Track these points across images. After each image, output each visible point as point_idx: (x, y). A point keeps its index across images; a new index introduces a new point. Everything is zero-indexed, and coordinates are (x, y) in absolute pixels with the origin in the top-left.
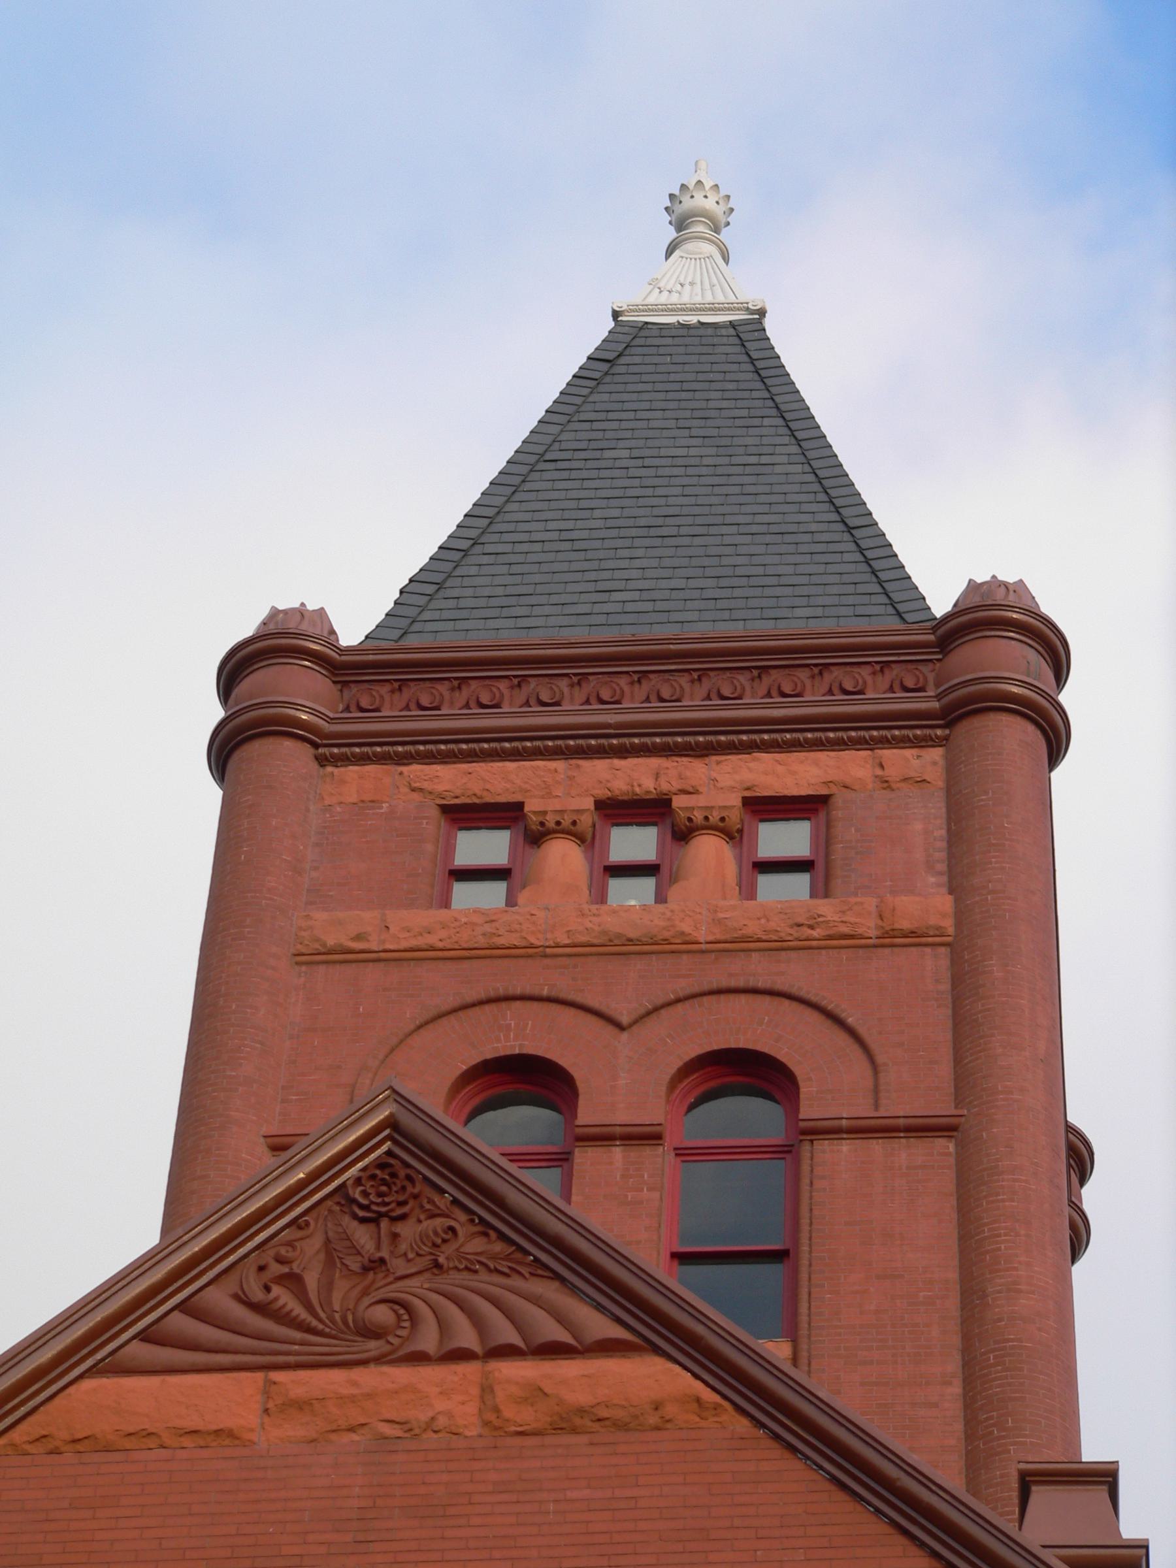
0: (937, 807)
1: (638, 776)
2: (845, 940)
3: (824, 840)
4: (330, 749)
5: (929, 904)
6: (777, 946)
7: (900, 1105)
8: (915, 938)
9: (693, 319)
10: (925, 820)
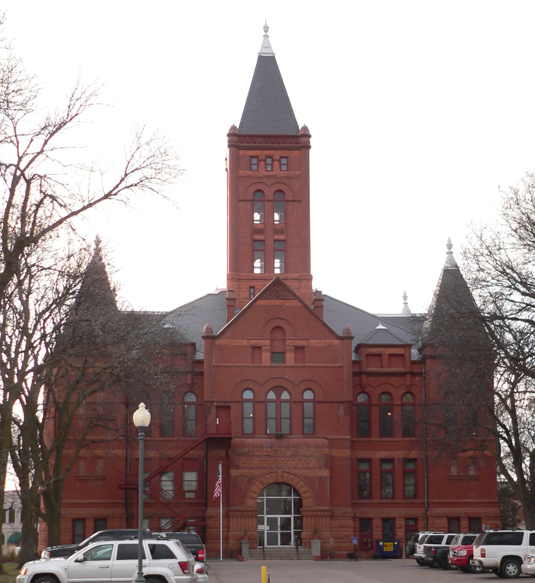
1: (267, 152)
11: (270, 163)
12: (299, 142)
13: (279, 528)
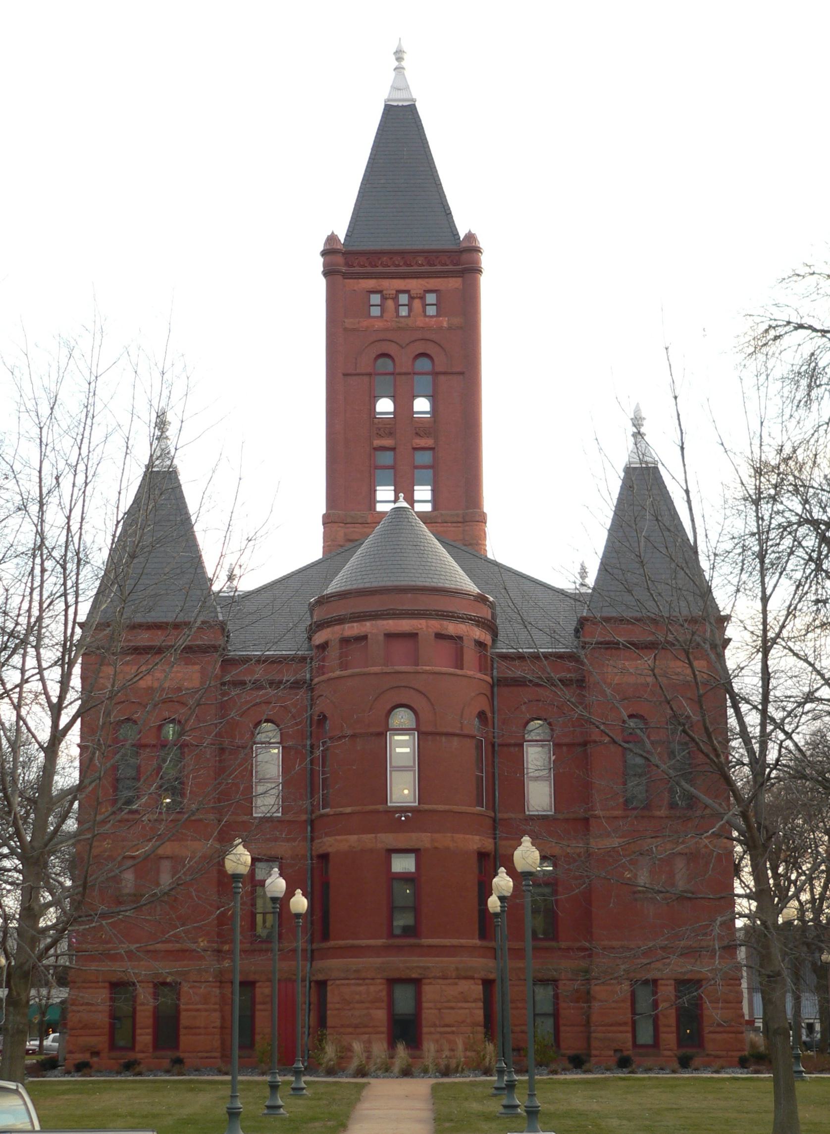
4: (346, 276)
9: (400, 104)
11: (407, 303)
12: (458, 262)
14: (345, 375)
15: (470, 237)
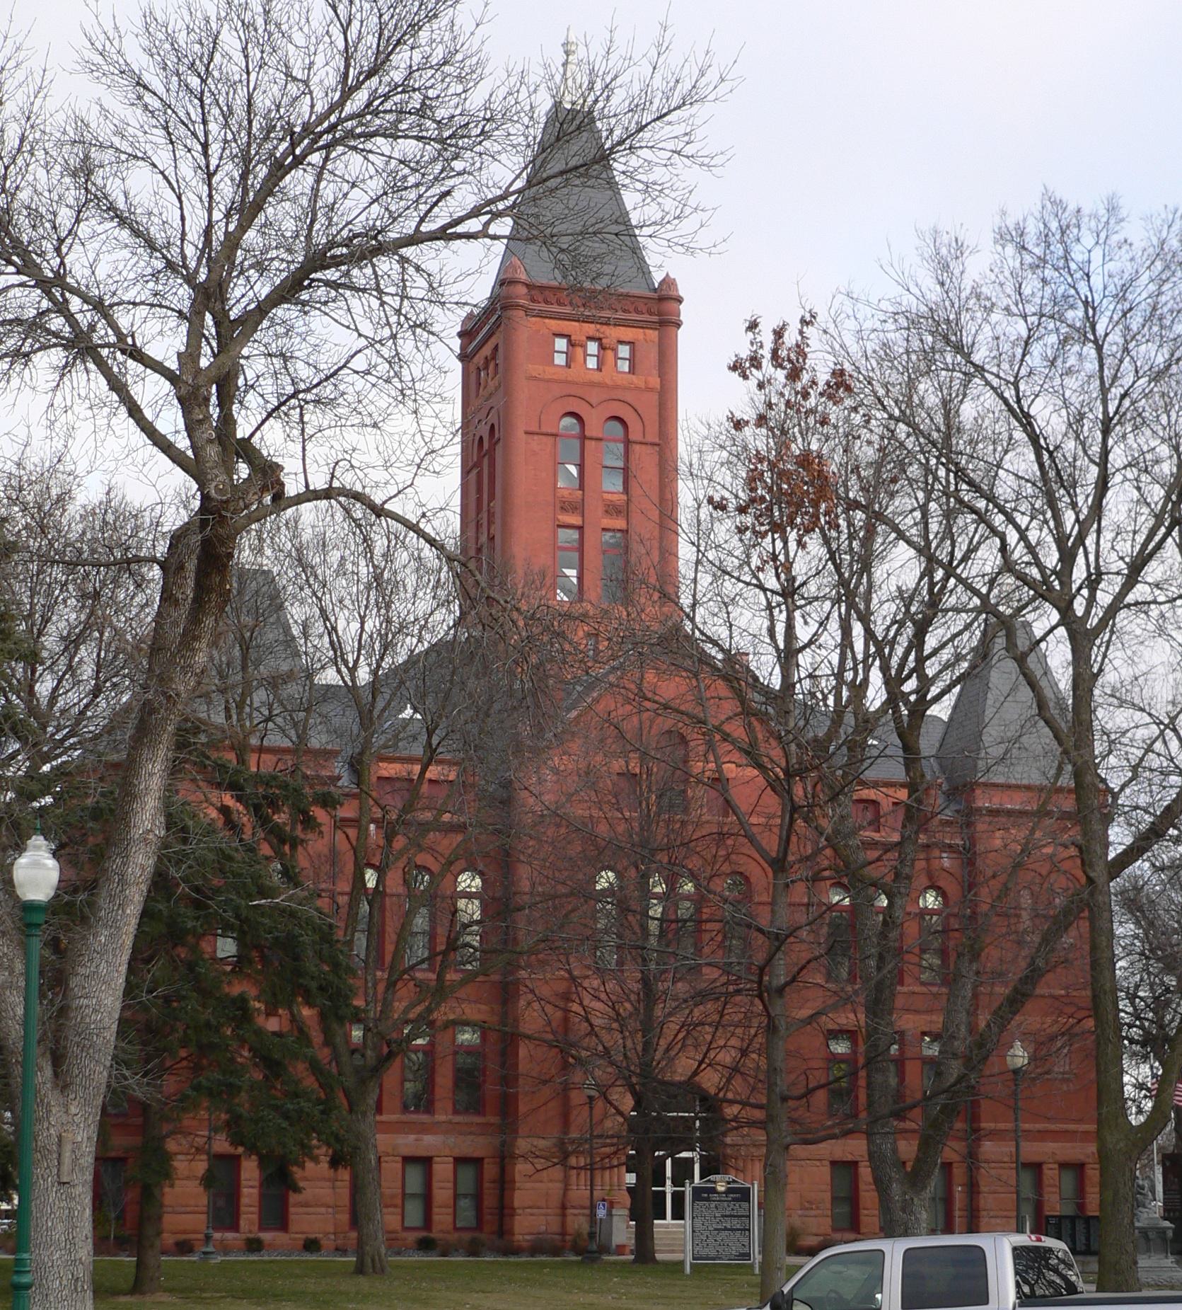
0: (656, 349)
2: (637, 388)
3: (633, 352)
5: (655, 381)
6: (625, 388)
7: (649, 439)
8: (652, 390)
10: (654, 355)
13: (669, 1182)
14: (526, 433)
15: (668, 282)
